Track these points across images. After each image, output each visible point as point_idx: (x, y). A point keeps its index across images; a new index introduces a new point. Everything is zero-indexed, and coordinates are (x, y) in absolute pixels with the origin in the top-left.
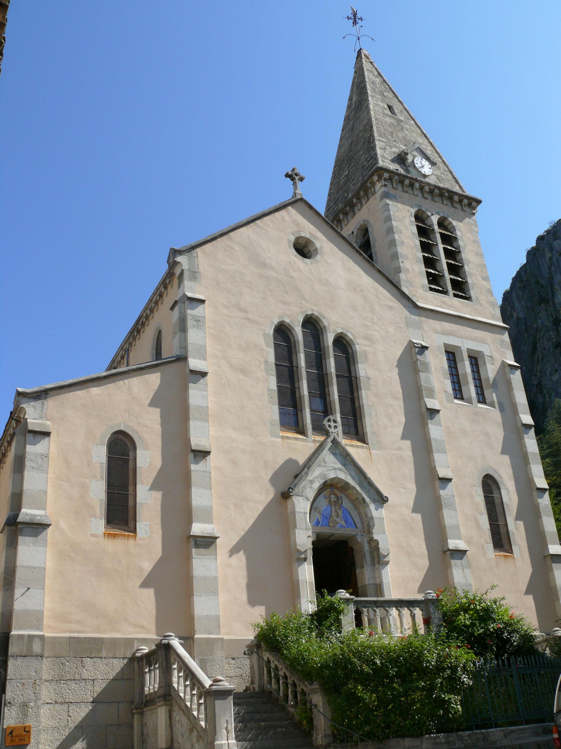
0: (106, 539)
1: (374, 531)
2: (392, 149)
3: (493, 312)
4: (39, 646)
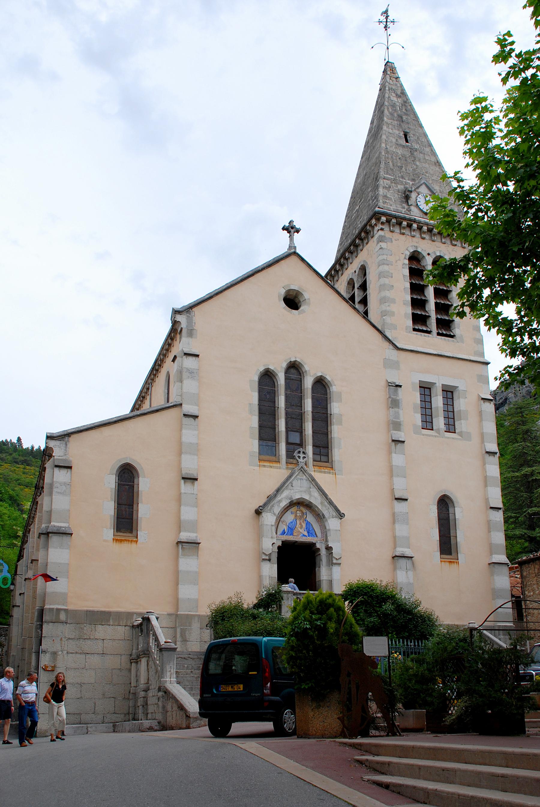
0: (115, 544)
2: (397, 187)
4: (65, 616)
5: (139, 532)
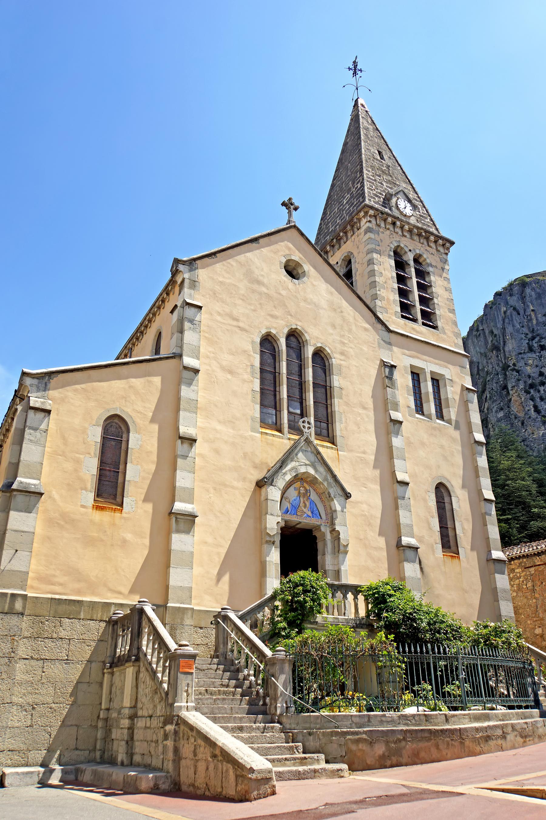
1: (337, 522)
3: (456, 341)
4: (21, 604)
5: (125, 499)
